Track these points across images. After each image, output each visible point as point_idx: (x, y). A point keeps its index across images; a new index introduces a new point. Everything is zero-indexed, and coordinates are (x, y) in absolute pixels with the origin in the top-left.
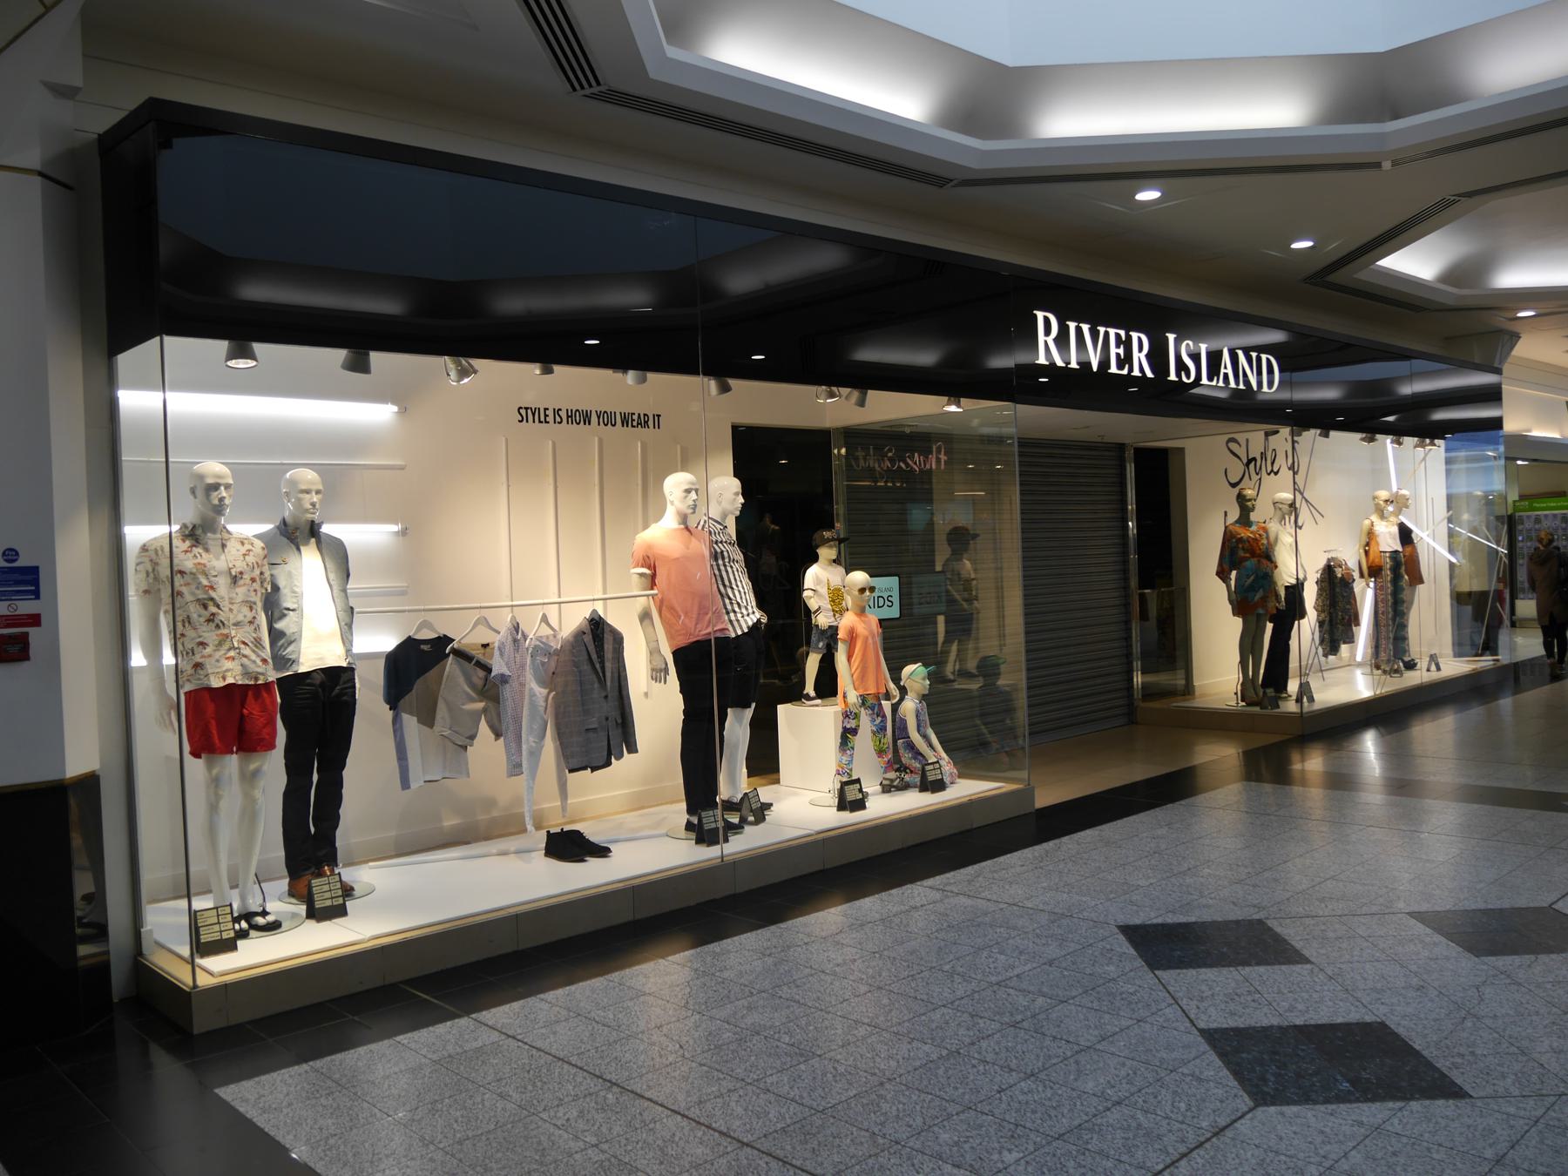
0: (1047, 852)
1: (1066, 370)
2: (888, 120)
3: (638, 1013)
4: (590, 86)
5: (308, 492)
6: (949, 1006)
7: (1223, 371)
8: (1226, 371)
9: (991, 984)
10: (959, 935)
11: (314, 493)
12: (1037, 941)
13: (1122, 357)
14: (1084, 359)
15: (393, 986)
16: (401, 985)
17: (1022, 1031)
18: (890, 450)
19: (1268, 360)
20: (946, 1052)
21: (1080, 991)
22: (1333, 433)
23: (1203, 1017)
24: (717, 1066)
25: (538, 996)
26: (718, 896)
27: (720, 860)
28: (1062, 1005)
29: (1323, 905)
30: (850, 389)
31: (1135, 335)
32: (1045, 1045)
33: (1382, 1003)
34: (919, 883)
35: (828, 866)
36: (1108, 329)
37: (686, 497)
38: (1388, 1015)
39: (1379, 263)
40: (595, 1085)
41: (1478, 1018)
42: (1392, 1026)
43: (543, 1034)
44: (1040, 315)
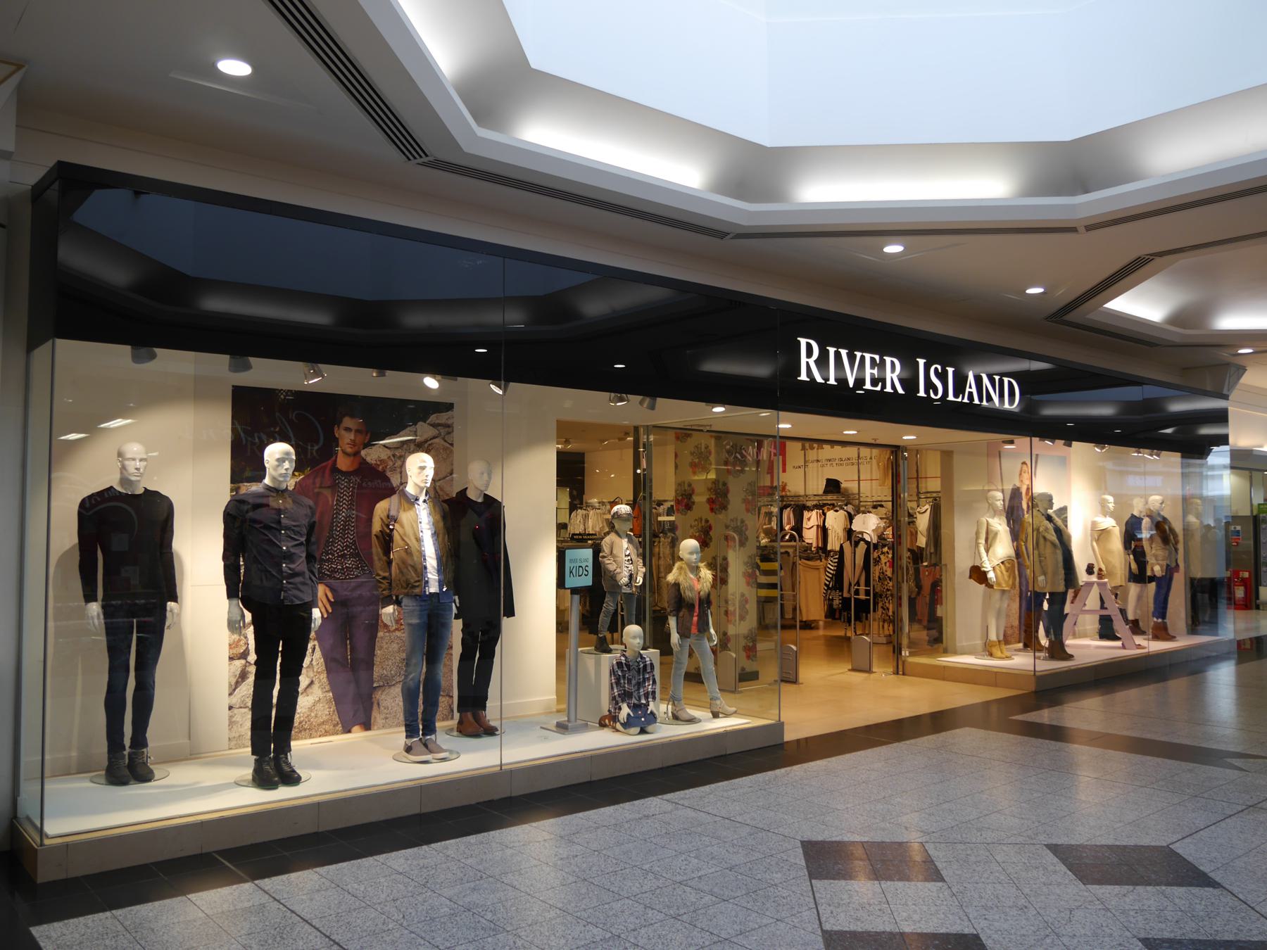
0: (776, 777)
1: (825, 386)
2: (667, 186)
3: (385, 888)
4: (421, 157)
5: (134, 459)
6: (632, 898)
7: (968, 390)
8: (970, 390)
9: (675, 882)
10: (670, 841)
11: (138, 461)
12: (731, 850)
13: (940, 371)
14: (841, 376)
15: (208, 855)
16: (214, 854)
17: (680, 922)
18: (728, 444)
19: (1009, 382)
20: (610, 934)
21: (744, 892)
22: (1075, 444)
23: (832, 921)
24: (423, 935)
25: (314, 869)
26: (496, 797)
27: (499, 768)
28: (722, 904)
29: (979, 834)
30: (642, 397)
31: (888, 360)
32: (691, 935)
33: (985, 919)
34: (660, 797)
35: (594, 779)
36: (864, 354)
37: (420, 473)
38: (985, 929)
39: (1105, 306)
40: (321, 943)
41: (1058, 936)
42: (983, 939)
43: (302, 900)
44: (803, 341)
